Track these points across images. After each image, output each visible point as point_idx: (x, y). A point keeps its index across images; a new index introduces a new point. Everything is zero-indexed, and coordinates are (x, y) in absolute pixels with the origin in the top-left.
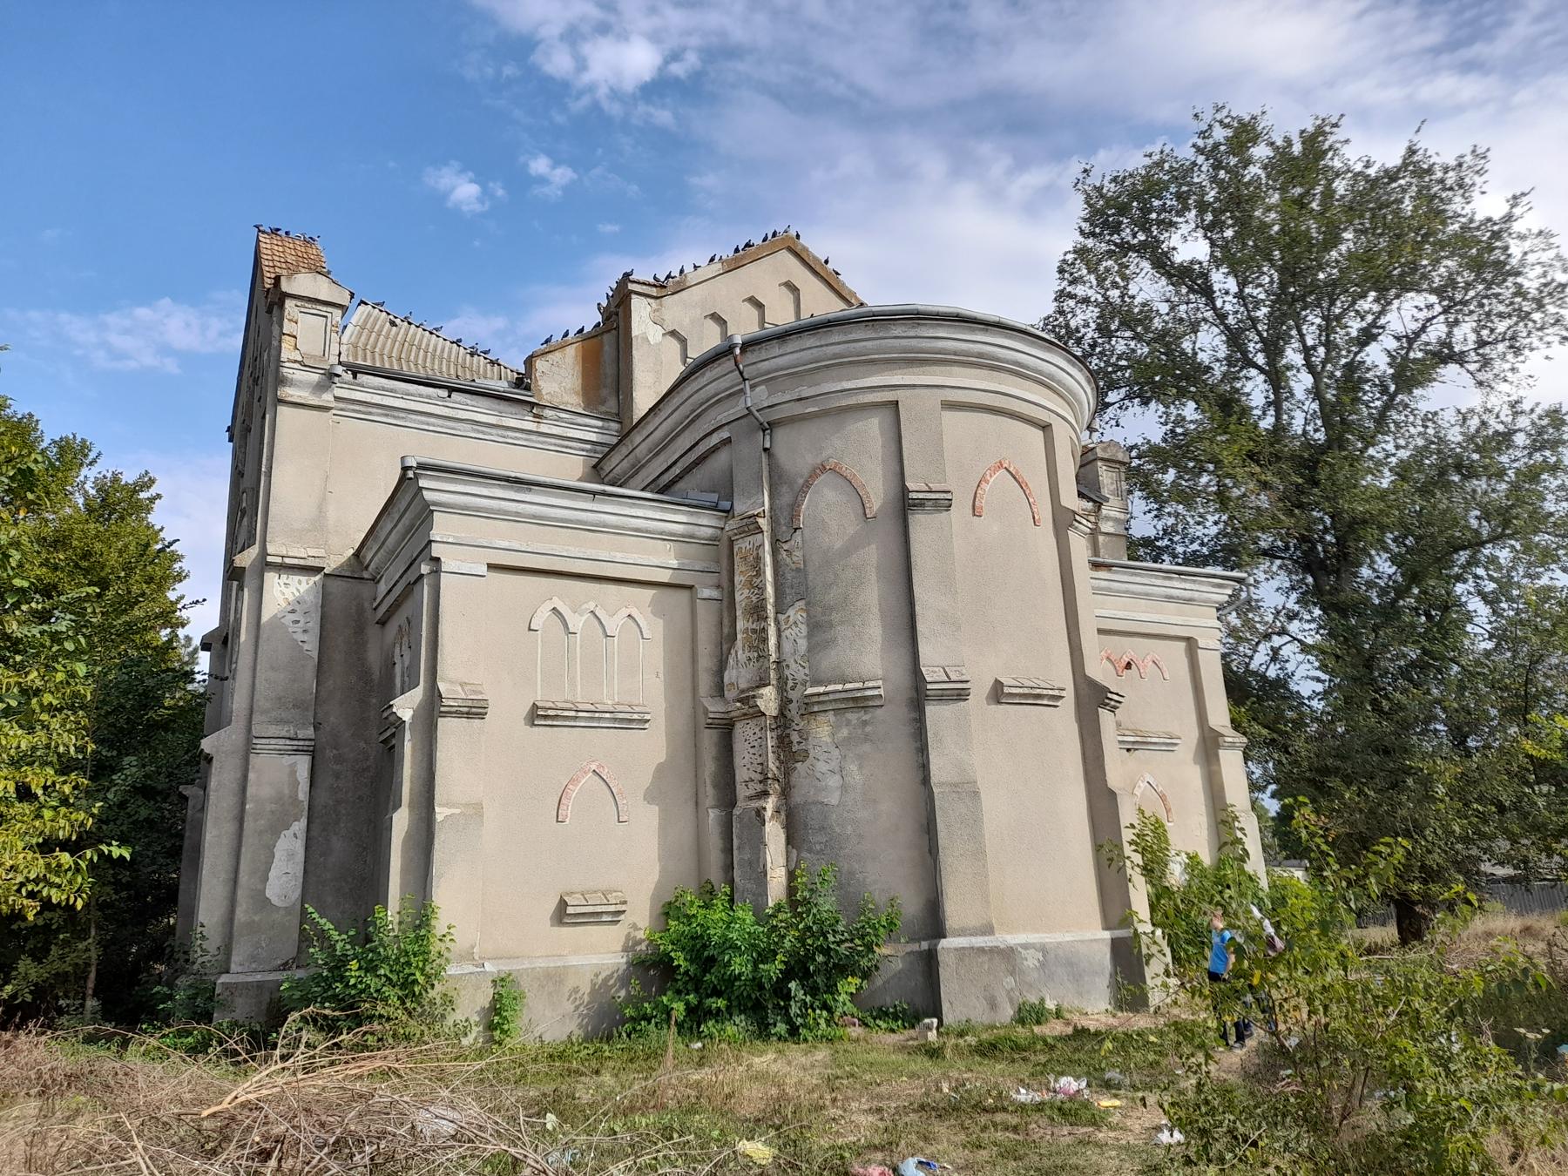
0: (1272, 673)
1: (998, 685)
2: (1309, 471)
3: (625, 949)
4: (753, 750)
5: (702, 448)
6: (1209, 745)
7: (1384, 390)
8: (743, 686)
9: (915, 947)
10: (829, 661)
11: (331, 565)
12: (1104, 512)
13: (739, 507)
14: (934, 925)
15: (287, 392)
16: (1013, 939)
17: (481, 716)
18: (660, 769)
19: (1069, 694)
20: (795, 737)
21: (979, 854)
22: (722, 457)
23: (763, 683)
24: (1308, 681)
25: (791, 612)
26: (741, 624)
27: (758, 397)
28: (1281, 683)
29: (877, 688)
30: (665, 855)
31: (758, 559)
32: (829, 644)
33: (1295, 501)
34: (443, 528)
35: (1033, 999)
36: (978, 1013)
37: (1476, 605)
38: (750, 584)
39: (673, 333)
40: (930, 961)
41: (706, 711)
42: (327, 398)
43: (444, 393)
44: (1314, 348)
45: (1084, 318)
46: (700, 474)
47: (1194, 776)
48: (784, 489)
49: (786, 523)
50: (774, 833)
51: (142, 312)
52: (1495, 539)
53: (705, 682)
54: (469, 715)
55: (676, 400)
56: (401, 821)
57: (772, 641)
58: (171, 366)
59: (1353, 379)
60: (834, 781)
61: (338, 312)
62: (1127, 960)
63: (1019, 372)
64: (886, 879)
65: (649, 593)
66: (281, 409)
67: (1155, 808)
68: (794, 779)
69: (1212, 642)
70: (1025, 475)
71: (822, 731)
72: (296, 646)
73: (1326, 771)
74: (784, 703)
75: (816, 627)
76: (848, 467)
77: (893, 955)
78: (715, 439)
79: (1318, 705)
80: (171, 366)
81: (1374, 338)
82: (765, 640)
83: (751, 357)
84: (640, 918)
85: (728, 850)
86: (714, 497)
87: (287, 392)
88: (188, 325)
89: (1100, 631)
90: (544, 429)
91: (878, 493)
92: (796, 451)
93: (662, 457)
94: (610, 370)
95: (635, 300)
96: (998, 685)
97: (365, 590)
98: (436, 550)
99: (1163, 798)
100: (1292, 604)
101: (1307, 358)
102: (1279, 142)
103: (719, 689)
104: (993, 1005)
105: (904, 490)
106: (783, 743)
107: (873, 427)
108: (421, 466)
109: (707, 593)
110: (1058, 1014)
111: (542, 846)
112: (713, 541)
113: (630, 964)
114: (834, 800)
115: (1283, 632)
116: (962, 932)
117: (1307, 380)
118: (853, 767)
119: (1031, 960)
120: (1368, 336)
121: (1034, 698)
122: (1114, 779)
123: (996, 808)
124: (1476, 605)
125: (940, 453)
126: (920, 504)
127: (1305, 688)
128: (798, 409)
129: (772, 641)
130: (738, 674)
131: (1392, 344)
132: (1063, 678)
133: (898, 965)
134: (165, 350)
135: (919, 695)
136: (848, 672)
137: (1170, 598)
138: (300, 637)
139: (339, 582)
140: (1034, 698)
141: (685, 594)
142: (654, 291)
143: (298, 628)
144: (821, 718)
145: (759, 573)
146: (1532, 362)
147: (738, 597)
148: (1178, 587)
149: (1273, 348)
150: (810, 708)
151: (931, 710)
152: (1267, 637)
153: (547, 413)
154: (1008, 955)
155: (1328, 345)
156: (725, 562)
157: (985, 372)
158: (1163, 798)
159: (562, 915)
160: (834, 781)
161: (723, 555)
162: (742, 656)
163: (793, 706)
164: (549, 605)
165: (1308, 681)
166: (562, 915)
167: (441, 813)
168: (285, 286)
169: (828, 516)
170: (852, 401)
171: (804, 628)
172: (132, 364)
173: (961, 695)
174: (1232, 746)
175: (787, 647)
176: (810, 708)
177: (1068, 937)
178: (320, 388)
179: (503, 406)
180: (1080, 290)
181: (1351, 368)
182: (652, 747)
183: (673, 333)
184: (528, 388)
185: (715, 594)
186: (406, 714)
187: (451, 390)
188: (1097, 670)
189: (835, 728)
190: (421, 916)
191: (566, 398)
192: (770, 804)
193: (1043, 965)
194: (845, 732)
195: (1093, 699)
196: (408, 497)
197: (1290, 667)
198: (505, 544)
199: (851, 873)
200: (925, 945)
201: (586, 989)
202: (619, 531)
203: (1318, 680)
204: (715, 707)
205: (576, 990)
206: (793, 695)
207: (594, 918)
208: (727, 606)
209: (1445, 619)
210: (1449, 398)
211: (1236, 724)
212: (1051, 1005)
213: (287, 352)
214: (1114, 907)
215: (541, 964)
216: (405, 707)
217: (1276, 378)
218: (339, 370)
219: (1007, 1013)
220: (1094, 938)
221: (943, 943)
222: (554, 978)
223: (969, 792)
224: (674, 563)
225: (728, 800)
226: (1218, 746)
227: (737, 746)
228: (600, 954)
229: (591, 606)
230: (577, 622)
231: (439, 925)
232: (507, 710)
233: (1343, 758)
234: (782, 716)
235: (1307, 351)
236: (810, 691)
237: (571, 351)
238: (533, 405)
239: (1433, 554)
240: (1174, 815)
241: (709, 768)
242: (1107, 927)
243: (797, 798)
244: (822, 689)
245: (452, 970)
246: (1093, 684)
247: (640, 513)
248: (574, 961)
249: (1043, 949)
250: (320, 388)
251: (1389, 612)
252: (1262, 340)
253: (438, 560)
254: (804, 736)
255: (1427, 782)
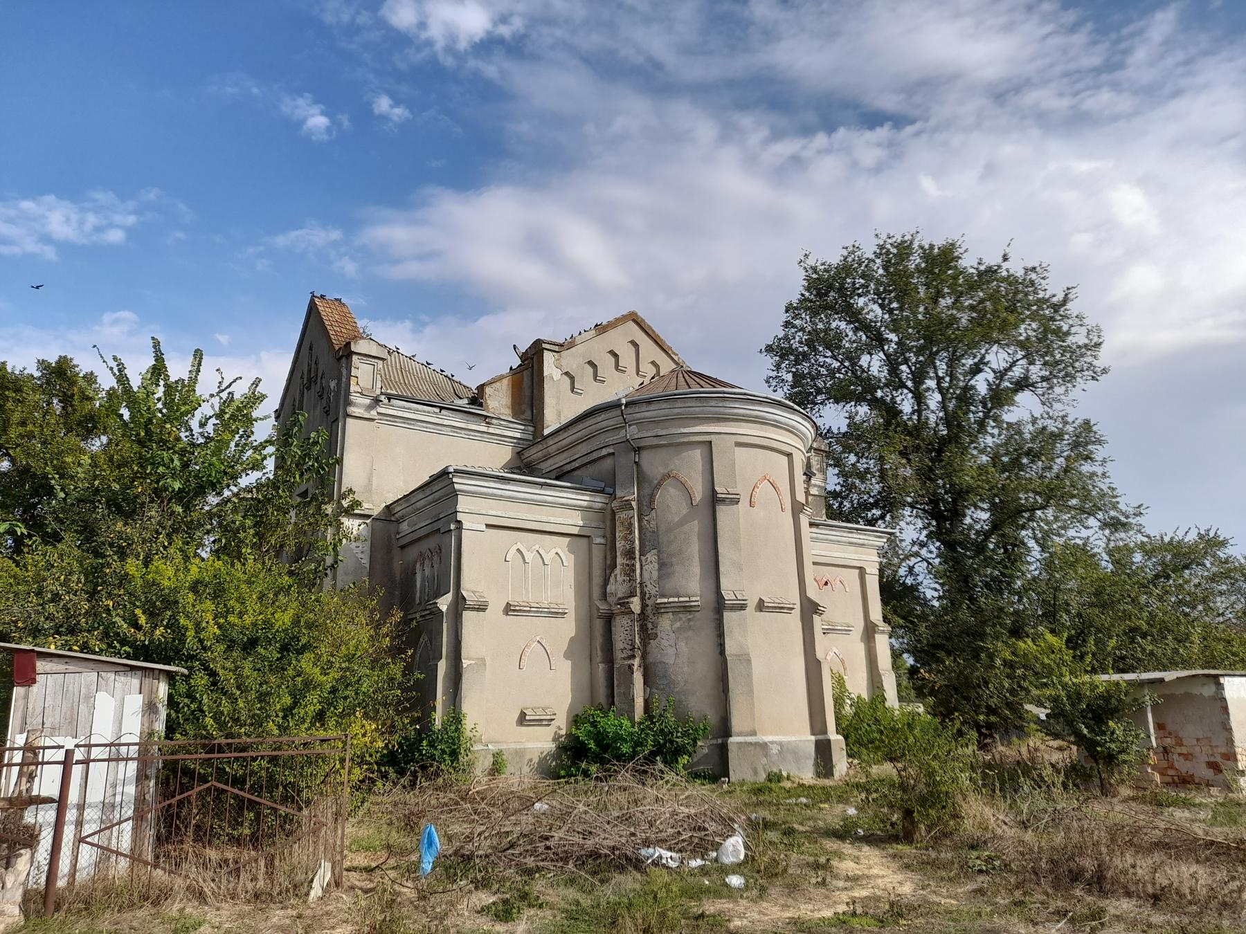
0: (909, 581)
1: (761, 601)
2: (937, 450)
3: (554, 740)
4: (623, 631)
5: (595, 455)
6: (870, 632)
7: (985, 406)
8: (620, 595)
9: (714, 742)
10: (669, 585)
11: (375, 513)
12: (813, 482)
13: (619, 493)
14: (725, 730)
15: (351, 410)
16: (768, 739)
17: (484, 610)
18: (572, 640)
19: (798, 607)
20: (650, 626)
21: (750, 692)
22: (608, 462)
23: (632, 595)
24: (931, 590)
25: (648, 555)
26: (619, 560)
27: (632, 432)
28: (914, 588)
29: (696, 600)
30: (575, 690)
31: (631, 524)
32: (668, 576)
33: (926, 475)
34: (463, 503)
35: (775, 770)
36: (749, 777)
37: (1031, 543)
38: (625, 539)
39: (567, 373)
40: (723, 750)
41: (598, 609)
42: (374, 413)
43: (437, 410)
44: (943, 378)
45: (798, 341)
46: (591, 469)
47: (860, 649)
48: (646, 485)
49: (647, 504)
50: (638, 677)
51: (27, 205)
52: (1043, 508)
53: (596, 591)
54: (478, 610)
55: (581, 426)
56: (442, 667)
57: (638, 572)
58: (50, 253)
59: (966, 397)
60: (671, 651)
61: (380, 362)
62: (823, 750)
63: (777, 425)
64: (700, 705)
65: (567, 540)
66: (349, 420)
67: (838, 668)
68: (649, 649)
69: (873, 570)
70: (778, 485)
71: (665, 624)
72: (358, 561)
73: (937, 647)
74: (644, 606)
75: (662, 565)
76: (684, 478)
77: (704, 747)
78: (604, 452)
79: (936, 603)
80: (50, 253)
81: (980, 371)
82: (634, 571)
83: (630, 410)
84: (561, 724)
85: (611, 686)
86: (603, 485)
87: (351, 410)
88: (68, 220)
89: (814, 563)
90: (491, 430)
91: (699, 492)
92: (653, 464)
93: (565, 455)
94: (527, 393)
95: (546, 353)
96: (761, 601)
97: (392, 527)
98: (460, 517)
99: (842, 661)
100: (923, 538)
101: (938, 384)
102: (927, 247)
103: (604, 596)
104: (756, 772)
105: (714, 492)
106: (643, 629)
107: (697, 454)
108: (456, 471)
109: (599, 540)
110: (788, 778)
111: (515, 681)
112: (601, 511)
113: (558, 748)
114: (671, 661)
115: (917, 554)
116: (740, 734)
117: (938, 397)
118: (682, 644)
119: (774, 750)
120: (976, 370)
121: (780, 609)
122: (820, 654)
123: (758, 669)
124: (1031, 543)
125: (734, 472)
126: (723, 501)
127: (929, 594)
128: (655, 441)
129: (638, 572)
130: (617, 586)
131: (991, 376)
132: (796, 599)
133: (706, 751)
134: (46, 239)
135: (719, 606)
136: (682, 591)
137: (851, 544)
138: (360, 556)
139: (378, 523)
140: (780, 609)
141: (586, 540)
142: (557, 348)
143: (358, 550)
144: (665, 616)
145: (631, 532)
146: (1075, 393)
147: (618, 545)
148: (856, 537)
149: (919, 377)
150: (658, 610)
151: (727, 615)
152: (907, 557)
153: (494, 421)
154: (764, 746)
155: (952, 376)
156: (608, 523)
157: (758, 426)
158: (842, 661)
159: (522, 720)
160: (671, 651)
161: (607, 521)
162: (620, 579)
163: (649, 608)
164: (515, 548)
165: (931, 590)
166: (522, 720)
167: (465, 663)
168: (353, 348)
169: (671, 503)
170: (686, 440)
171: (656, 565)
172: (16, 250)
173: (742, 607)
174: (883, 632)
175: (646, 575)
176: (658, 610)
177: (793, 739)
178: (370, 408)
179: (470, 417)
180: (797, 322)
181: (967, 389)
182: (567, 628)
183: (567, 373)
184: (481, 405)
185: (602, 541)
186: (444, 608)
187: (441, 408)
188: (812, 593)
189: (673, 622)
190: (456, 718)
191: (503, 411)
192: (636, 662)
193: (780, 752)
194: (678, 624)
195: (810, 609)
196: (441, 485)
197: (920, 578)
198: (494, 513)
199: (680, 702)
200: (720, 741)
201: (536, 760)
202: (553, 505)
203: (936, 590)
204: (603, 607)
205: (531, 760)
206: (649, 602)
207: (539, 722)
208: (611, 552)
209: (1013, 554)
210: (1024, 409)
211: (885, 619)
212: (785, 774)
213: (353, 388)
214: (817, 724)
215: (513, 746)
216: (444, 603)
217: (919, 397)
218: (382, 398)
219: (762, 777)
220: (806, 739)
221: (731, 740)
222: (519, 753)
223: (746, 659)
224: (581, 523)
225: (609, 659)
226: (875, 632)
227: (615, 627)
228: (541, 742)
229: (537, 547)
230: (529, 556)
231: (468, 724)
232: (496, 608)
233: (948, 639)
234: (643, 616)
235: (939, 380)
236: (659, 601)
237: (505, 382)
238: (486, 417)
239: (1008, 515)
240: (848, 672)
241: (599, 640)
242: (813, 734)
243: (650, 659)
244: (666, 600)
245: (476, 747)
246: (810, 601)
247: (565, 495)
248: (529, 745)
249: (781, 744)
250: (370, 408)
251: (980, 548)
252: (912, 372)
253: (460, 522)
254: (655, 626)
255: (991, 657)
